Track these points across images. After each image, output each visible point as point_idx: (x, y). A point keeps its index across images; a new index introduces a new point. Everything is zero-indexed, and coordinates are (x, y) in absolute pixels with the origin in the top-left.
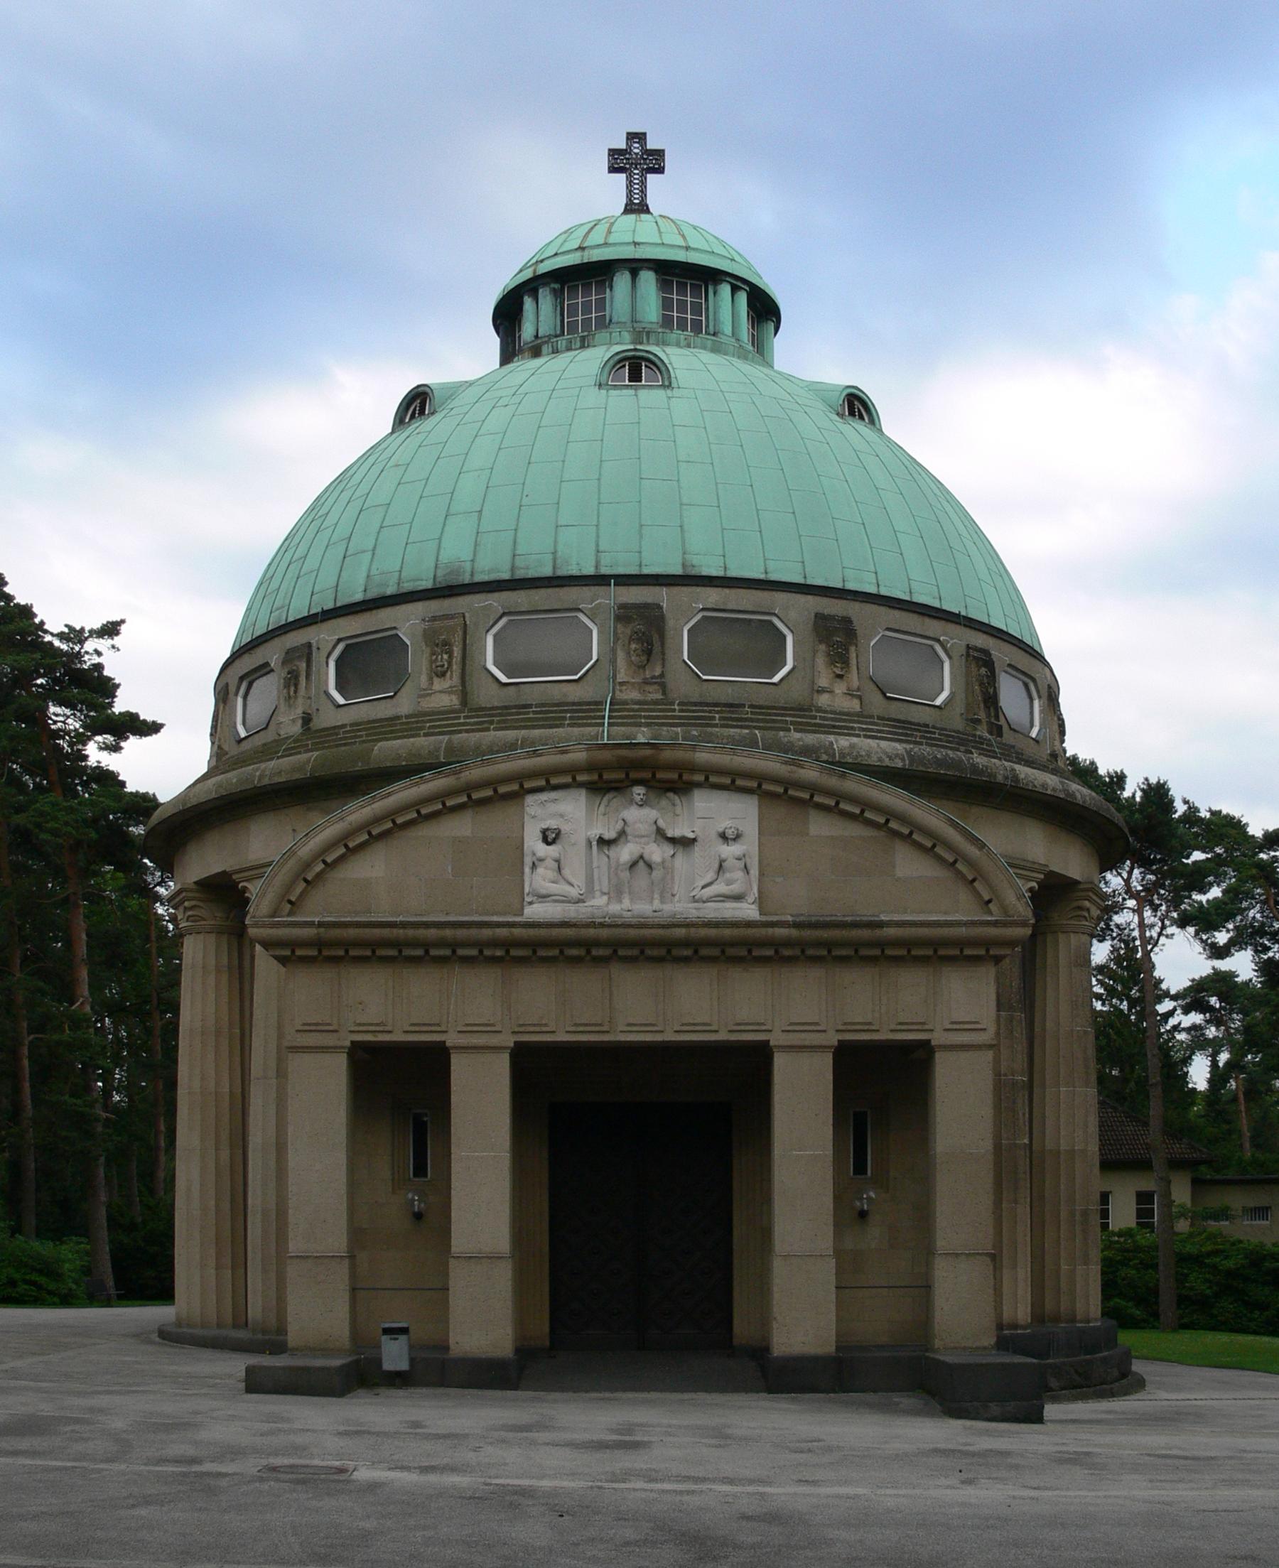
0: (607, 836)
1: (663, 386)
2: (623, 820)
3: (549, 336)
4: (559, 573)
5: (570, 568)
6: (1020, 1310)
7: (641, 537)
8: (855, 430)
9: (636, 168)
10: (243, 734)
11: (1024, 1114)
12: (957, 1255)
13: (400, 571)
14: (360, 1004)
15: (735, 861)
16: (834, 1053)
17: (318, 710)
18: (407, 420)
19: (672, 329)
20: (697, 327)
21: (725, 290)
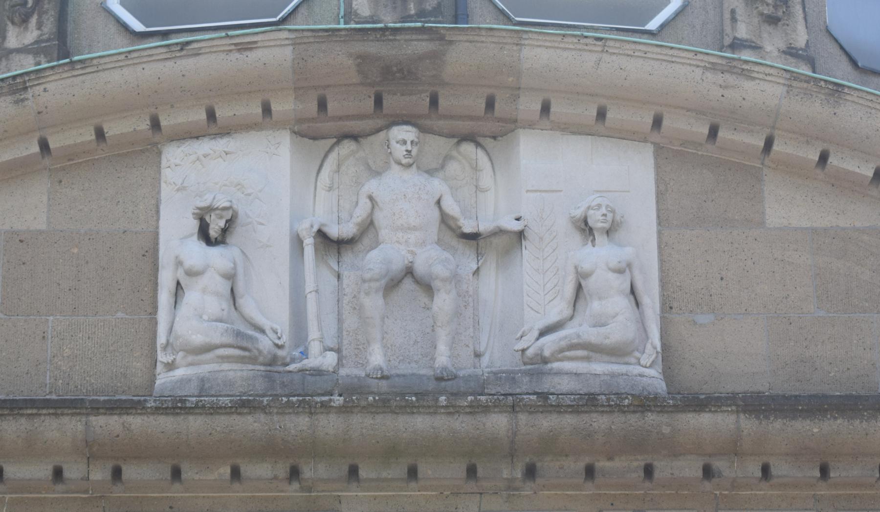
0: (334, 232)
2: (371, 198)
15: (611, 276)
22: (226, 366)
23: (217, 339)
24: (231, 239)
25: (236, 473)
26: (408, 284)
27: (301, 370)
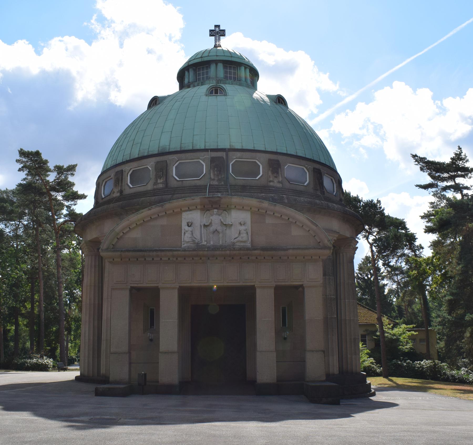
0: (206, 224)
1: (224, 95)
2: (211, 219)
3: (193, 82)
4: (194, 148)
5: (197, 147)
6: (335, 370)
7: (218, 137)
8: (279, 107)
9: (217, 35)
10: (103, 197)
11: (334, 308)
12: (313, 351)
13: (149, 149)
14: (133, 275)
15: (244, 231)
16: (274, 289)
17: (125, 189)
18: (152, 106)
19: (227, 80)
20: (235, 79)
21: (243, 68)
22: (191, 244)
23: (190, 241)
24: (192, 226)
25: (193, 259)
26: (216, 232)
27: (202, 245)
